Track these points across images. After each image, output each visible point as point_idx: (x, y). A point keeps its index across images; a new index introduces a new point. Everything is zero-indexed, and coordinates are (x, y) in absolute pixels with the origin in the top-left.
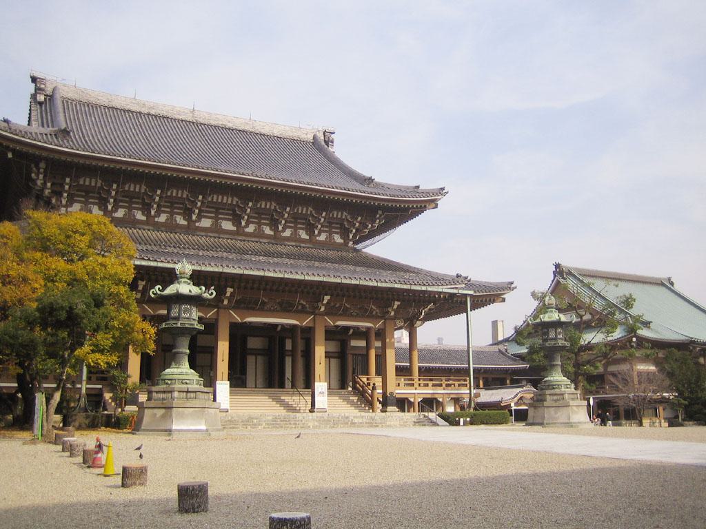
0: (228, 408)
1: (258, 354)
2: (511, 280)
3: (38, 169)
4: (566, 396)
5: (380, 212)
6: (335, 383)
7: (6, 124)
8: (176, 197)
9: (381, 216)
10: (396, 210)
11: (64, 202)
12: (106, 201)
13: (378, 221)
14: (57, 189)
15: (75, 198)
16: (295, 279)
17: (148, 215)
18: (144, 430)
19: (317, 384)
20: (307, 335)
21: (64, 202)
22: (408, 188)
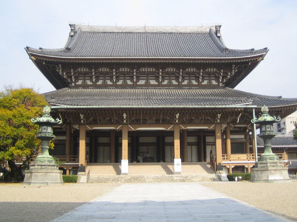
0: (128, 173)
1: (193, 145)
2: (280, 96)
3: (59, 67)
4: (269, 164)
5: (234, 66)
6: (88, 160)
7: (40, 50)
8: (211, 72)
9: (235, 67)
10: (245, 64)
11: (73, 80)
12: (179, 77)
13: (234, 71)
14: (69, 75)
15: (80, 78)
16: (148, 108)
17: (198, 82)
18: (25, 183)
19: (175, 160)
20: (118, 135)
21: (73, 80)
22: (248, 50)
